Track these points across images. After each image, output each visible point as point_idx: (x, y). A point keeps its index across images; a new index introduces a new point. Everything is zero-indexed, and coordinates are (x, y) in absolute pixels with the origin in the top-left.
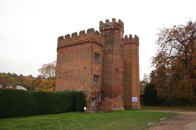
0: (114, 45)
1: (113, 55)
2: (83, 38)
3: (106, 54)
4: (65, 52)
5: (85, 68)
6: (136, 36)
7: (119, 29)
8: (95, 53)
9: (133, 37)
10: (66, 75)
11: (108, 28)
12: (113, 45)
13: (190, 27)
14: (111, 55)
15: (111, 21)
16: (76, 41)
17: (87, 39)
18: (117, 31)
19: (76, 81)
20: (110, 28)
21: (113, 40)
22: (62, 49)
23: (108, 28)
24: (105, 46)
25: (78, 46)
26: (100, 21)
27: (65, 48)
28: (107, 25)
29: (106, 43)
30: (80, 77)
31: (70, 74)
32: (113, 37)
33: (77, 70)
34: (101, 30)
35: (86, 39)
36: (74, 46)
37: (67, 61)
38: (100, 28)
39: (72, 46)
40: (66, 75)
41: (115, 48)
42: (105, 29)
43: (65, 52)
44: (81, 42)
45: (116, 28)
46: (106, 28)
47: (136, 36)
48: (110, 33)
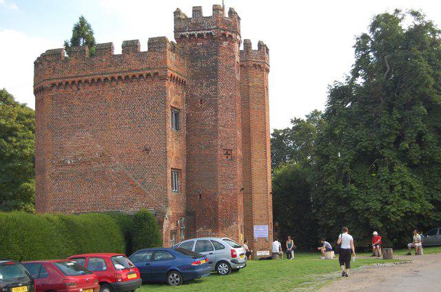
0: (220, 83)
1: (217, 111)
2: (135, 63)
3: (198, 109)
4: (76, 102)
5: (147, 150)
6: (261, 45)
7: (230, 36)
8: (172, 107)
9: (255, 47)
10: (82, 168)
11: (192, 33)
12: (215, 84)
13: (420, 33)
14: (210, 111)
15: (207, 12)
16: (112, 69)
17: (149, 68)
18: (225, 44)
19: (118, 186)
20: (207, 34)
21: (215, 69)
22: (61, 90)
23: (200, 32)
24: (192, 86)
25: (121, 86)
26: (175, 10)
27: (75, 88)
28: (197, 24)
29: (195, 77)
30: (130, 175)
31: (96, 166)
32: (216, 61)
33: (121, 156)
34: (180, 37)
35: (145, 66)
36: (108, 84)
37: (82, 127)
38: (176, 31)
39: (100, 86)
40: (82, 168)
41: (222, 93)
42: (190, 35)
43: (76, 102)
44: (130, 75)
45: (224, 35)
46: (196, 33)
47: (261, 45)
48: (207, 47)
